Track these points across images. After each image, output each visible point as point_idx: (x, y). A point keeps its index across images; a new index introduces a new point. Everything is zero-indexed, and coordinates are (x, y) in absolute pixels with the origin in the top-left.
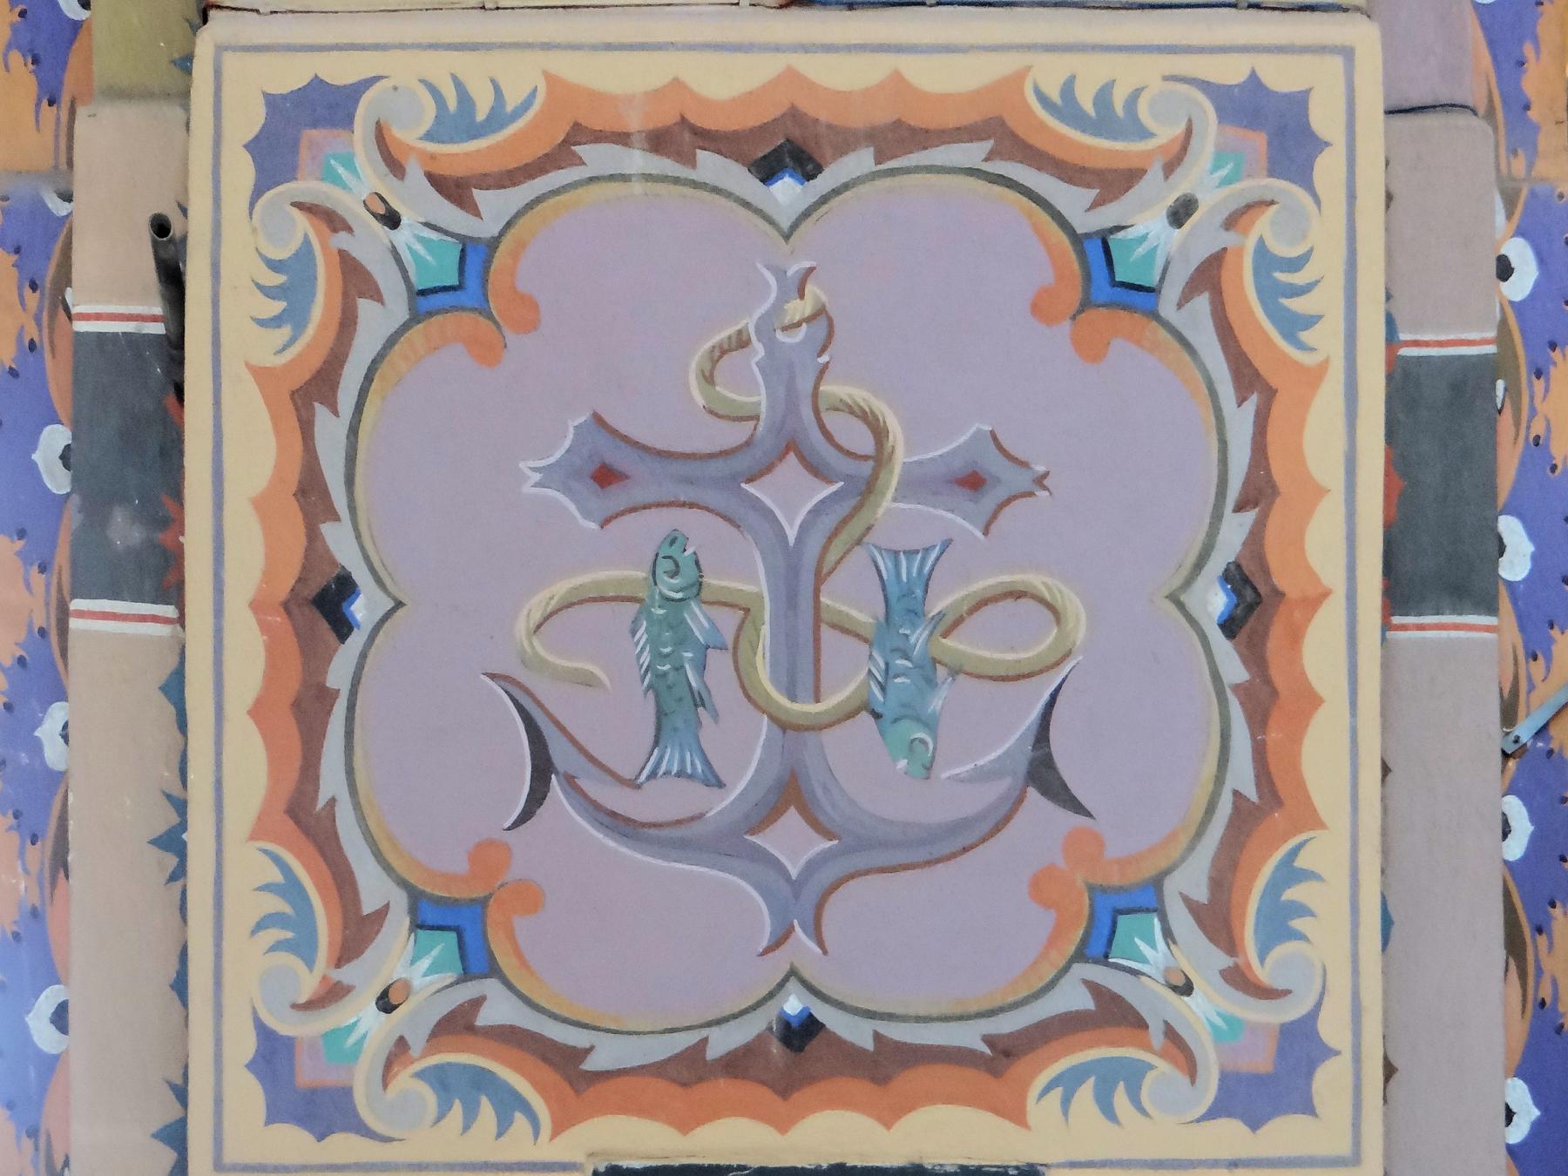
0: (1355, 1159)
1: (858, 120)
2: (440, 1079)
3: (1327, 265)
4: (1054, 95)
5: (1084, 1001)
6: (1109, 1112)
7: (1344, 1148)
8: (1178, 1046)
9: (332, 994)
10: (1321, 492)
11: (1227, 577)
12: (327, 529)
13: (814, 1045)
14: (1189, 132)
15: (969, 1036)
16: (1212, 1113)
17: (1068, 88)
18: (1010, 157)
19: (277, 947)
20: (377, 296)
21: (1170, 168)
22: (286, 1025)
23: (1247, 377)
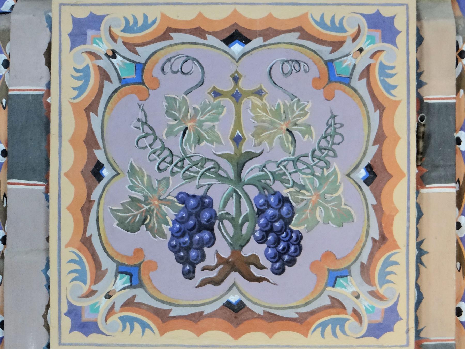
0: (61, 5)
1: (258, 28)
2: (342, 29)
3: (66, 279)
4: (318, 19)
5: (328, 302)
6: (134, 17)
7: (405, 343)
8: (357, 314)
9: (91, 293)
10: (68, 208)
11: (367, 167)
12: (375, 203)
13: (243, 314)
14: (106, 320)
15: (292, 314)
16: (104, 16)
17: (322, 17)
18: (164, 310)
19: (74, 280)
20: (134, 297)
21: (354, 40)
22: (77, 303)
23: (379, 106)
